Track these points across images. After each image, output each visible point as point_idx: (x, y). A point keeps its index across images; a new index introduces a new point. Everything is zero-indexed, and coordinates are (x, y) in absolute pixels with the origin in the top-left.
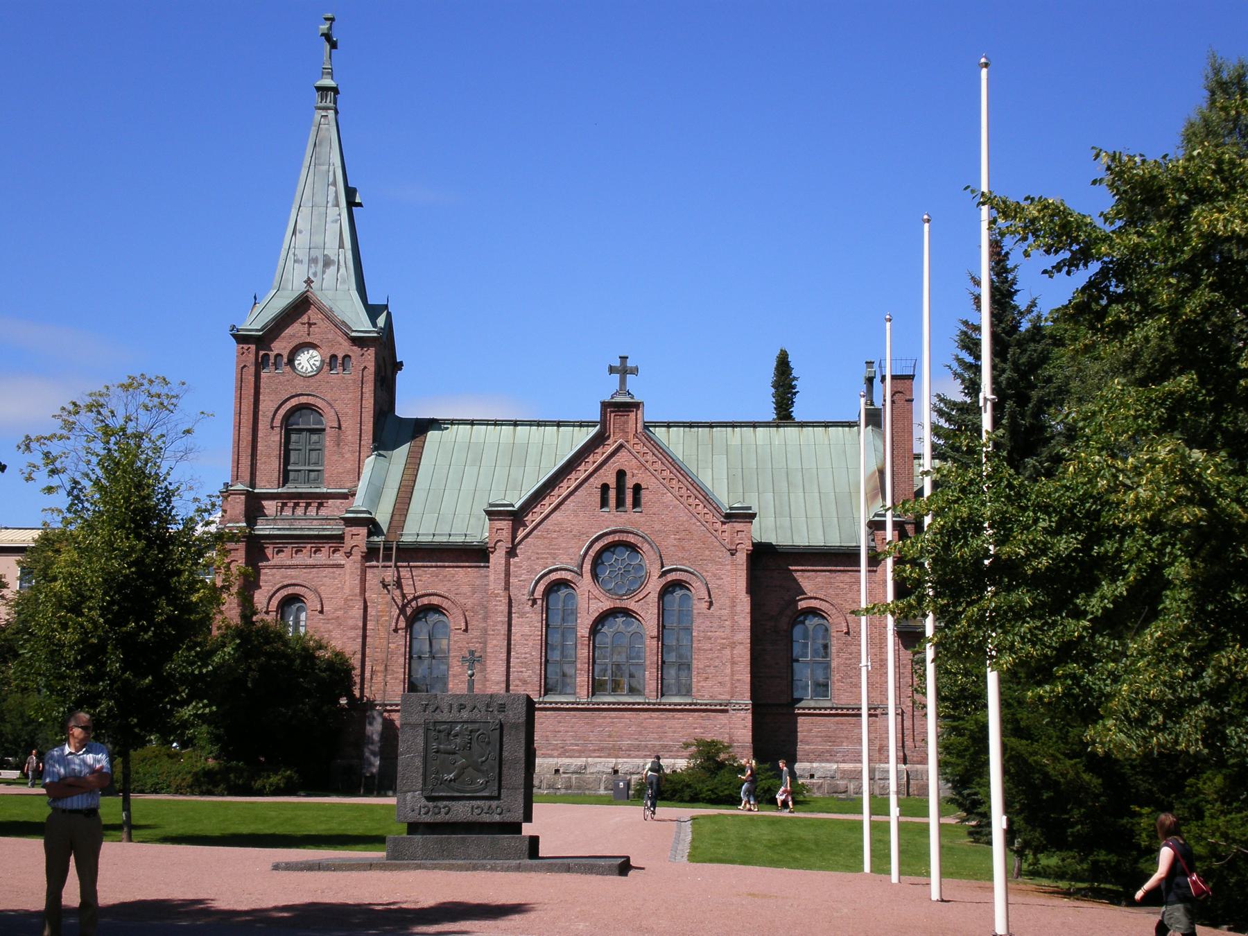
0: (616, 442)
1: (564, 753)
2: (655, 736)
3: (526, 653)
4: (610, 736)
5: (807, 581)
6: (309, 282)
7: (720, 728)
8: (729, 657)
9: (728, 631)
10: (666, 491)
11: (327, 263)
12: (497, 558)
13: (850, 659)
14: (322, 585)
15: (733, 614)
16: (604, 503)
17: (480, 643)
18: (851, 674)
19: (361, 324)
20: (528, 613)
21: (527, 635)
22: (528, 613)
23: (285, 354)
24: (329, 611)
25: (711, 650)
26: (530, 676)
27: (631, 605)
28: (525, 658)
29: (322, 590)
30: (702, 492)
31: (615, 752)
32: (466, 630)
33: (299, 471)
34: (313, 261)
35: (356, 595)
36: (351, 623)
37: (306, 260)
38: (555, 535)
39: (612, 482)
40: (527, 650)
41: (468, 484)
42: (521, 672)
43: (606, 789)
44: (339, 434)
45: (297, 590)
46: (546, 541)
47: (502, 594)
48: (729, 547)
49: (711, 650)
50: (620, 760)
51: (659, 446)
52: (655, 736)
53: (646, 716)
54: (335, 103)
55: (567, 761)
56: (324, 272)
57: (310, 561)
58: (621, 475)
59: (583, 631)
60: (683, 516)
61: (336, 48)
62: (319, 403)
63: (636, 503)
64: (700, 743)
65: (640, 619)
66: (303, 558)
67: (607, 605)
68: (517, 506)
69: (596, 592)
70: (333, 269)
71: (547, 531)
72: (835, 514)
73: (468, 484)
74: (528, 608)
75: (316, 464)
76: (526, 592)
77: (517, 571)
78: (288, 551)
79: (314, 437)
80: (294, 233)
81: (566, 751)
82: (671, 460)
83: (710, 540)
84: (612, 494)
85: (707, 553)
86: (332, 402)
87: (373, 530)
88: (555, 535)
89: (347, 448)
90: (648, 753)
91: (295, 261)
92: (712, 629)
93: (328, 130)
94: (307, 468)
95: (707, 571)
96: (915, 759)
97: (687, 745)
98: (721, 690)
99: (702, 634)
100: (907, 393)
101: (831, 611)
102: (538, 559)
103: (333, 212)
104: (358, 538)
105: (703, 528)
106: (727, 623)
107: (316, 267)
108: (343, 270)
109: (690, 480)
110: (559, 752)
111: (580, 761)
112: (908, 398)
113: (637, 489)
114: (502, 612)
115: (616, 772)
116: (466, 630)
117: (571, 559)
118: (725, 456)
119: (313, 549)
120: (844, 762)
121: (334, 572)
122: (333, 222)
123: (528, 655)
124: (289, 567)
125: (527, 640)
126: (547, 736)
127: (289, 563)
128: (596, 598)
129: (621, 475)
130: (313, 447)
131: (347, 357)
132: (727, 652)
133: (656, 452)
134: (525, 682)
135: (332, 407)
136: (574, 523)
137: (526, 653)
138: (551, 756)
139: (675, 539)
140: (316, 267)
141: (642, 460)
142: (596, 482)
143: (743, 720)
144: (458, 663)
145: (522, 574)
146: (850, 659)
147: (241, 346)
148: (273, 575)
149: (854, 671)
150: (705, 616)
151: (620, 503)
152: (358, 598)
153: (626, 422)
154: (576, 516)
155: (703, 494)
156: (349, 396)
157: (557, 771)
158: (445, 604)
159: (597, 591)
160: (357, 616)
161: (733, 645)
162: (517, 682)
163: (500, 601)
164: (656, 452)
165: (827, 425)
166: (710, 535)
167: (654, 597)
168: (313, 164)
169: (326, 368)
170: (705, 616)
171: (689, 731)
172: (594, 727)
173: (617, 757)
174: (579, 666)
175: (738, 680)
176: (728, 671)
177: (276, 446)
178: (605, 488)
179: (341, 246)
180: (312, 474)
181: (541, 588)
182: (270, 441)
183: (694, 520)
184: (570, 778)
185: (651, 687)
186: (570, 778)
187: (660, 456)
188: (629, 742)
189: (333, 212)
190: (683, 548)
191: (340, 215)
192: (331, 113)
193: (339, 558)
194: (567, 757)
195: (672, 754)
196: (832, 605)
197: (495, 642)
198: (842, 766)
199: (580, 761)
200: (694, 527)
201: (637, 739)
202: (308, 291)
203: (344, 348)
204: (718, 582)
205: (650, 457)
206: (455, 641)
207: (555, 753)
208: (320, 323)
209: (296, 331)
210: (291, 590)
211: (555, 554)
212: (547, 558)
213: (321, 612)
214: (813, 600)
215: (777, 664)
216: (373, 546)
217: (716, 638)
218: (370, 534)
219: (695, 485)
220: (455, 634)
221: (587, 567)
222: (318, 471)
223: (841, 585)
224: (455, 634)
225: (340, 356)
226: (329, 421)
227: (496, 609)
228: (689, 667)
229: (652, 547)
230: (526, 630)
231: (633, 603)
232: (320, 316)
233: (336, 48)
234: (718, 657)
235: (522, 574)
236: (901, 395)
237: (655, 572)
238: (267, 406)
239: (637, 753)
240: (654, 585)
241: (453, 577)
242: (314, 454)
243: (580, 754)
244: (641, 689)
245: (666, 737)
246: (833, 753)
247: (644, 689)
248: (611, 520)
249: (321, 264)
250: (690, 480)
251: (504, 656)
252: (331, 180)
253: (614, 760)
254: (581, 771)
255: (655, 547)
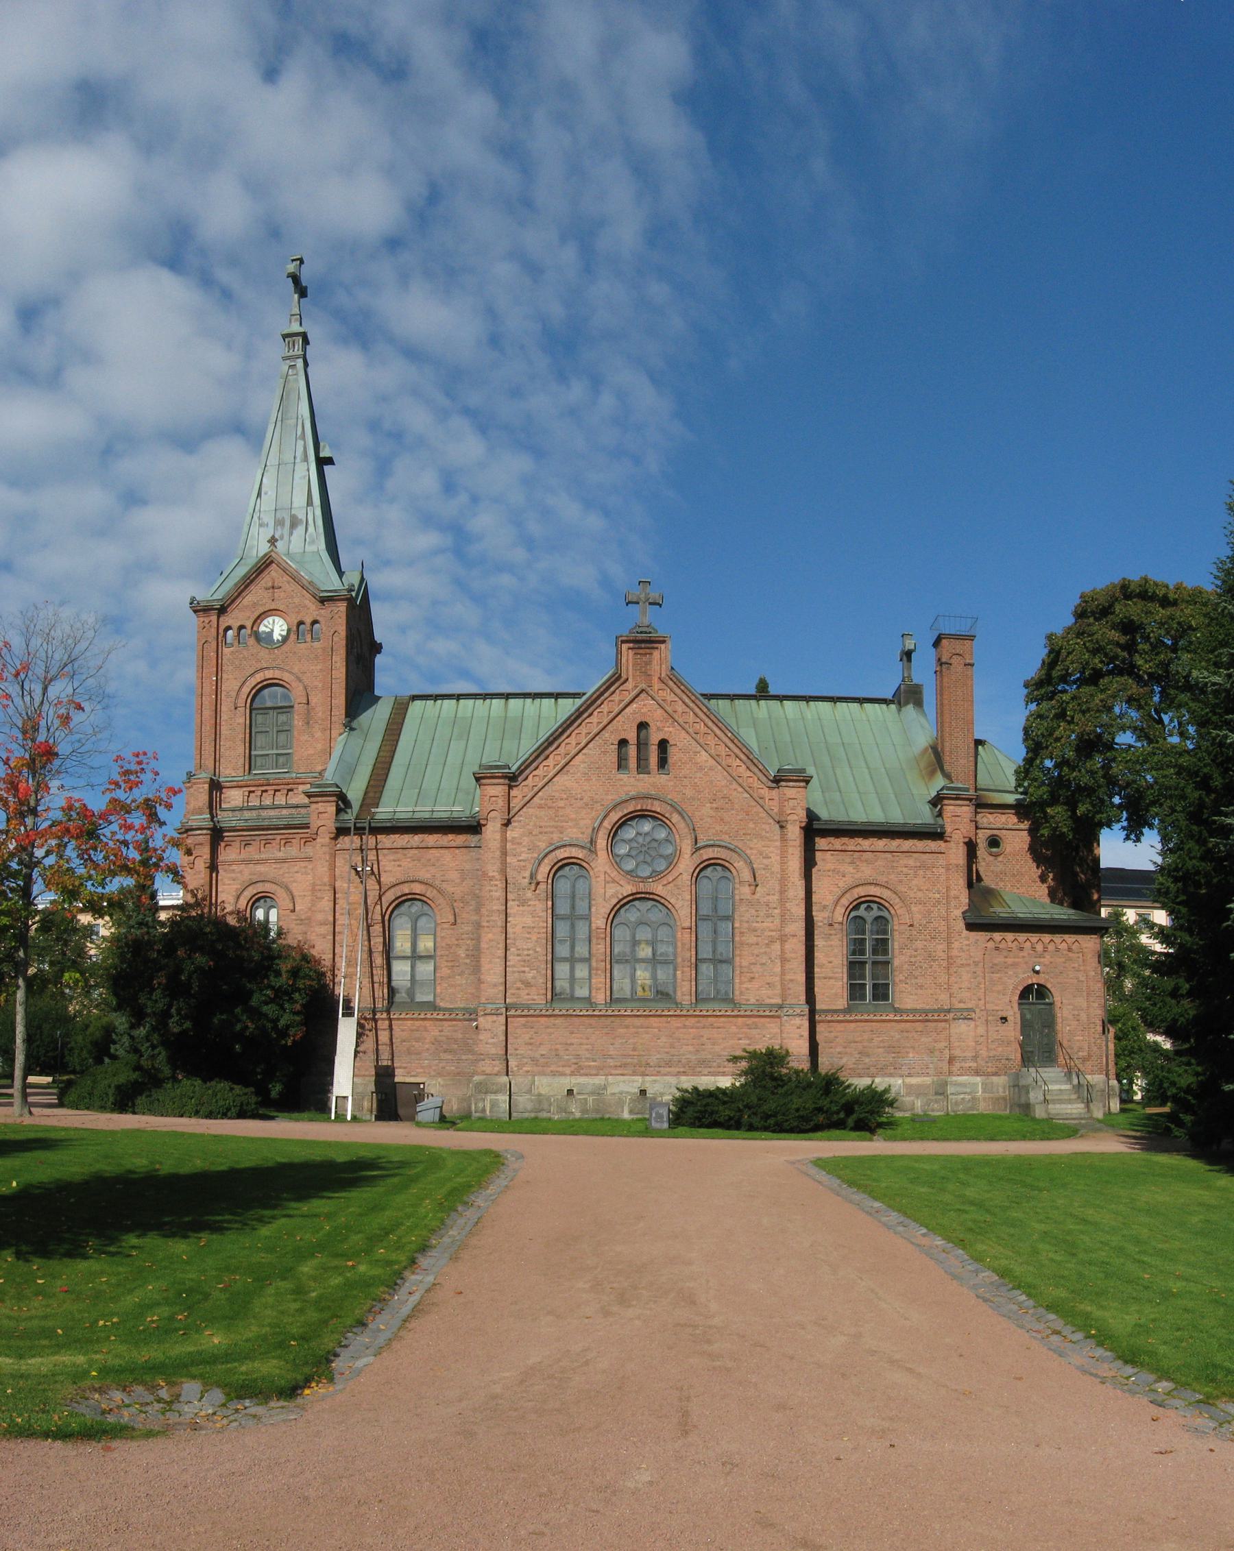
0: (636, 687)
1: (578, 1071)
2: (691, 1048)
3: (528, 950)
4: (634, 1049)
5: (865, 864)
6: (273, 541)
7: (770, 1039)
8: (779, 953)
9: (777, 921)
10: (699, 748)
11: (294, 523)
12: (492, 830)
13: (915, 957)
14: (294, 881)
15: (783, 901)
16: (621, 764)
17: (472, 939)
18: (916, 973)
19: (330, 582)
20: (530, 900)
21: (529, 927)
22: (530, 900)
23: (249, 624)
24: (301, 910)
25: (757, 944)
26: (534, 978)
27: (658, 888)
28: (528, 955)
29: (293, 887)
30: (744, 750)
31: (641, 1068)
32: (455, 924)
33: (267, 755)
34: (279, 523)
35: (325, 885)
36: (320, 917)
37: (272, 524)
38: (561, 804)
39: (632, 736)
40: (530, 945)
41: (454, 758)
42: (524, 972)
43: (631, 1112)
44: (308, 711)
45: (268, 887)
46: (551, 812)
47: (498, 877)
48: (777, 818)
49: (757, 944)
50: (648, 1078)
51: (690, 692)
52: (691, 1048)
53: (679, 1025)
54: (304, 350)
55: (582, 1080)
56: (291, 534)
57: (280, 855)
58: (642, 726)
59: (599, 922)
60: (720, 777)
61: (306, 296)
62: (286, 677)
63: (663, 762)
64: (753, 1055)
65: (670, 906)
66: (274, 852)
67: (628, 889)
68: (514, 769)
69: (614, 874)
70: (300, 530)
71: (552, 798)
72: (890, 791)
73: (454, 758)
74: (529, 894)
75: (284, 747)
76: (527, 874)
77: (515, 849)
78: (255, 844)
79: (282, 718)
80: (259, 495)
81: (581, 1068)
82: (705, 710)
83: (755, 810)
84: (632, 751)
85: (751, 825)
86: (300, 675)
87: (342, 806)
88: (561, 804)
89: (317, 726)
90: (682, 1070)
91: (260, 525)
92: (758, 919)
93: (297, 380)
94: (275, 752)
95: (751, 849)
96: (989, 1070)
97: (735, 1059)
98: (770, 992)
99: (746, 925)
100: (967, 656)
101: (895, 900)
102: (541, 833)
103: (301, 468)
104: (324, 815)
105: (746, 795)
106: (776, 911)
107: (282, 529)
108: (311, 529)
109: (729, 735)
110: (572, 1069)
111: (599, 1080)
112: (968, 661)
113: (663, 745)
114: (498, 899)
115: (643, 1092)
116: (455, 924)
117: (583, 833)
118: (753, 730)
119: (283, 842)
120: (910, 1075)
121: (306, 867)
122: (300, 478)
123: (531, 952)
124: (258, 862)
125: (529, 933)
126: (557, 1050)
127: (257, 857)
128: (614, 881)
129: (642, 726)
130: (281, 728)
131: (315, 622)
132: (777, 947)
133: (687, 700)
134: (528, 984)
135: (300, 681)
136: (585, 788)
137: (528, 950)
138: (563, 1074)
139: (711, 808)
140: (282, 529)
141: (669, 709)
142: (611, 736)
143: (798, 1028)
144: (446, 964)
145: (522, 852)
146: (915, 957)
147: (202, 619)
148: (241, 872)
149: (920, 970)
150: (750, 903)
151: (642, 767)
152: (327, 888)
153: (649, 663)
154: (589, 780)
155: (747, 752)
156: (319, 667)
157: (570, 1092)
158: (430, 893)
159: (615, 873)
160: (327, 909)
161: (783, 939)
162: (519, 985)
163: (496, 885)
164: (687, 700)
165: (861, 701)
166: (754, 803)
167: (686, 877)
168: (279, 418)
169: (293, 637)
170: (750, 903)
171: (731, 1042)
172: (614, 1039)
173: (644, 1075)
174: (594, 964)
175: (792, 980)
176: (778, 969)
177: (240, 729)
178: (623, 743)
179: (310, 502)
180: (281, 759)
181: (544, 869)
182: (234, 722)
183: (735, 785)
184: (586, 1100)
185: (684, 989)
186: (586, 1100)
187: (691, 705)
188: (658, 1056)
189: (301, 468)
190: (722, 820)
191: (308, 470)
192: (300, 362)
193: (309, 850)
194: (581, 1075)
195: (712, 1070)
196: (895, 893)
197: (490, 936)
198: (908, 1080)
199: (599, 1080)
200: (735, 793)
201: (667, 1053)
202: (272, 551)
203: (312, 610)
204: (765, 861)
205: (680, 707)
206: (442, 937)
207: (568, 1070)
208: (286, 587)
209: (256, 595)
210: (260, 887)
211: (562, 827)
212: (552, 833)
213: (293, 911)
214: (873, 887)
215: (830, 962)
216: (343, 825)
217: (763, 930)
218: (339, 811)
219: (736, 741)
220: (442, 929)
221: (602, 842)
222: (288, 754)
223: (905, 870)
224: (442, 929)
225: (308, 621)
226: (297, 695)
227: (491, 896)
228: (729, 961)
229: (683, 818)
230: (528, 921)
231: (660, 887)
232: (286, 578)
233: (306, 296)
234: (765, 953)
235: (522, 852)
236: (960, 658)
237: (687, 847)
238: (230, 683)
239: (668, 1069)
240: (686, 865)
241: (438, 860)
242: (282, 737)
243: (598, 1071)
244: (671, 993)
245: (704, 1050)
246: (897, 1066)
247: (675, 992)
248: (632, 783)
249: (288, 523)
250: (729, 735)
251: (501, 953)
252: (299, 433)
253: (639, 1079)
254: (599, 1091)
255: (686, 817)
